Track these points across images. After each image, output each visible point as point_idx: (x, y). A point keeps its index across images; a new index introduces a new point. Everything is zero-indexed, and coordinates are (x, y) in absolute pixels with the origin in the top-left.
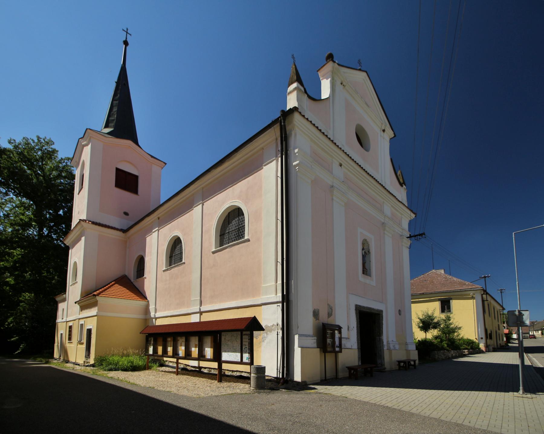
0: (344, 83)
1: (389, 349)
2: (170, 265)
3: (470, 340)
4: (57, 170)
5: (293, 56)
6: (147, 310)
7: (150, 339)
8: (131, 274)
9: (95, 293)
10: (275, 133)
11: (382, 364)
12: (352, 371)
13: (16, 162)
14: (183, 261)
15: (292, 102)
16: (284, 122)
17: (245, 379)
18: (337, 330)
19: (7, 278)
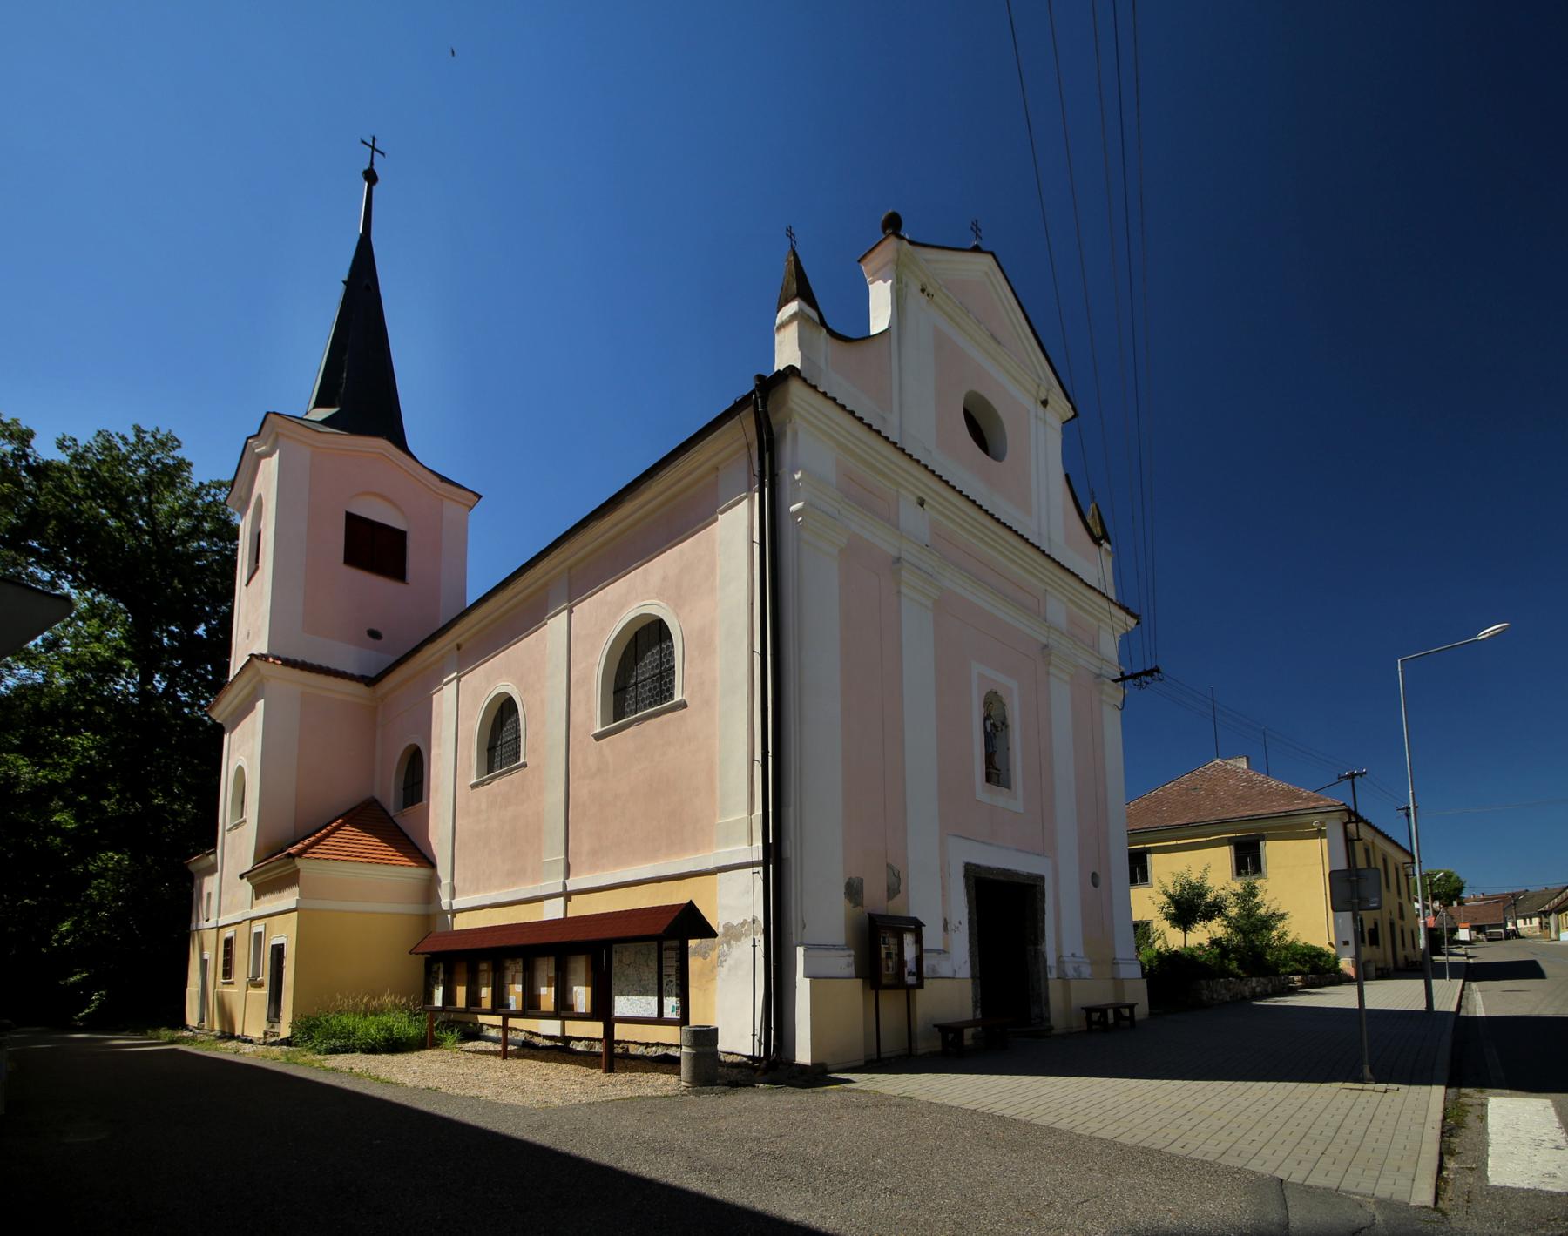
0: (929, 289)
1: (1062, 977)
2: (490, 770)
3: (1314, 948)
4: (188, 515)
5: (789, 229)
6: (430, 889)
7: (435, 967)
8: (388, 792)
9: (292, 850)
10: (743, 430)
11: (1044, 1018)
12: (951, 1036)
13: (76, 497)
14: (522, 760)
15: (787, 352)
16: (764, 405)
17: (668, 1063)
18: (909, 930)
19: (54, 812)
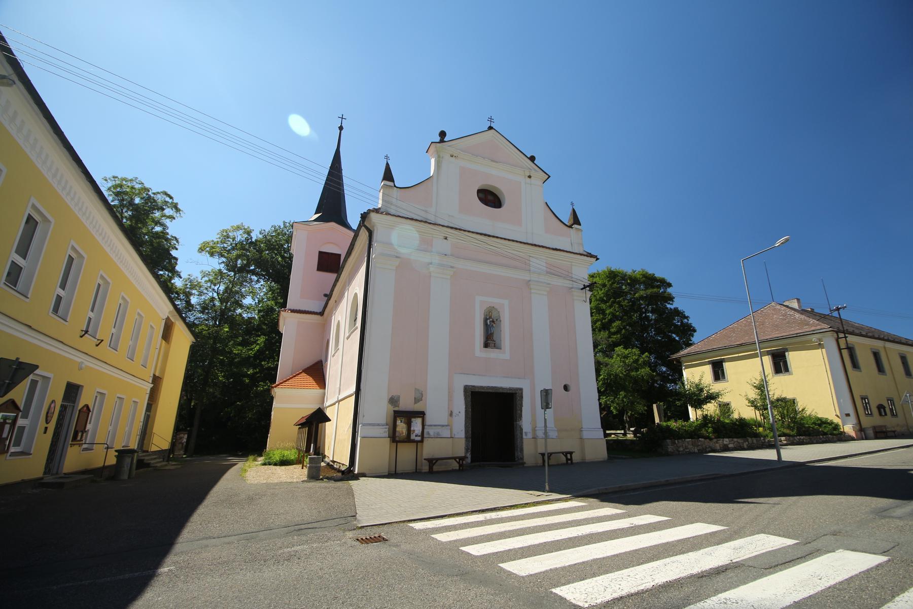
3: (820, 419)
